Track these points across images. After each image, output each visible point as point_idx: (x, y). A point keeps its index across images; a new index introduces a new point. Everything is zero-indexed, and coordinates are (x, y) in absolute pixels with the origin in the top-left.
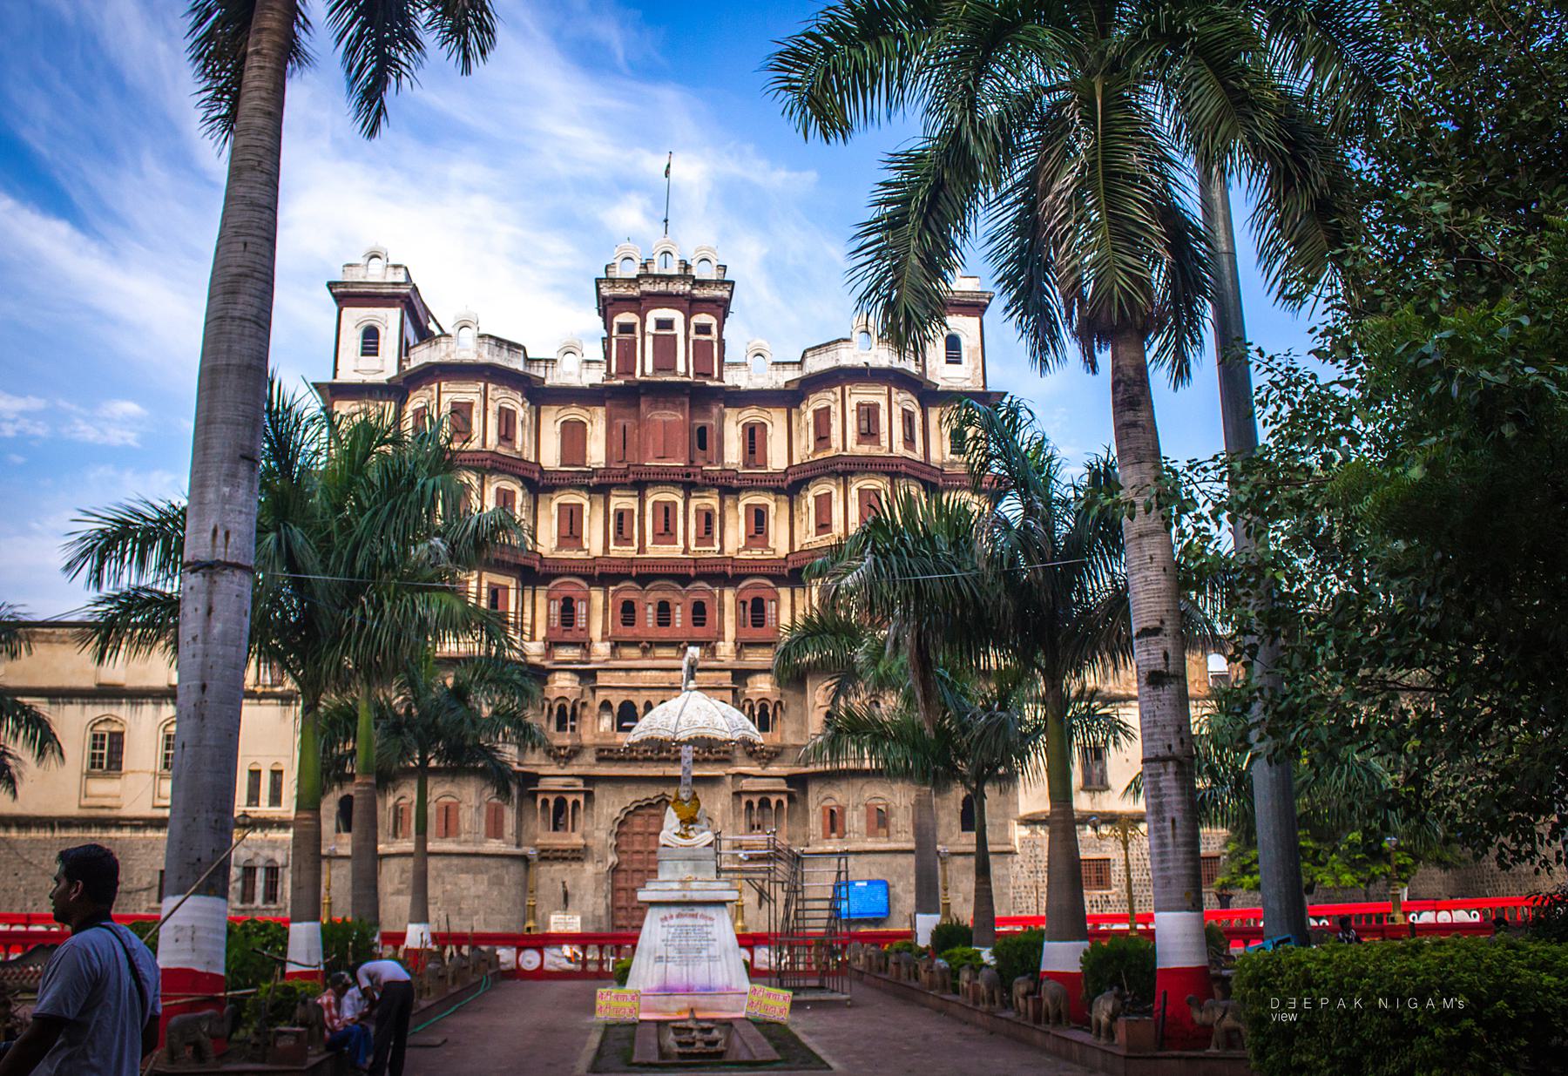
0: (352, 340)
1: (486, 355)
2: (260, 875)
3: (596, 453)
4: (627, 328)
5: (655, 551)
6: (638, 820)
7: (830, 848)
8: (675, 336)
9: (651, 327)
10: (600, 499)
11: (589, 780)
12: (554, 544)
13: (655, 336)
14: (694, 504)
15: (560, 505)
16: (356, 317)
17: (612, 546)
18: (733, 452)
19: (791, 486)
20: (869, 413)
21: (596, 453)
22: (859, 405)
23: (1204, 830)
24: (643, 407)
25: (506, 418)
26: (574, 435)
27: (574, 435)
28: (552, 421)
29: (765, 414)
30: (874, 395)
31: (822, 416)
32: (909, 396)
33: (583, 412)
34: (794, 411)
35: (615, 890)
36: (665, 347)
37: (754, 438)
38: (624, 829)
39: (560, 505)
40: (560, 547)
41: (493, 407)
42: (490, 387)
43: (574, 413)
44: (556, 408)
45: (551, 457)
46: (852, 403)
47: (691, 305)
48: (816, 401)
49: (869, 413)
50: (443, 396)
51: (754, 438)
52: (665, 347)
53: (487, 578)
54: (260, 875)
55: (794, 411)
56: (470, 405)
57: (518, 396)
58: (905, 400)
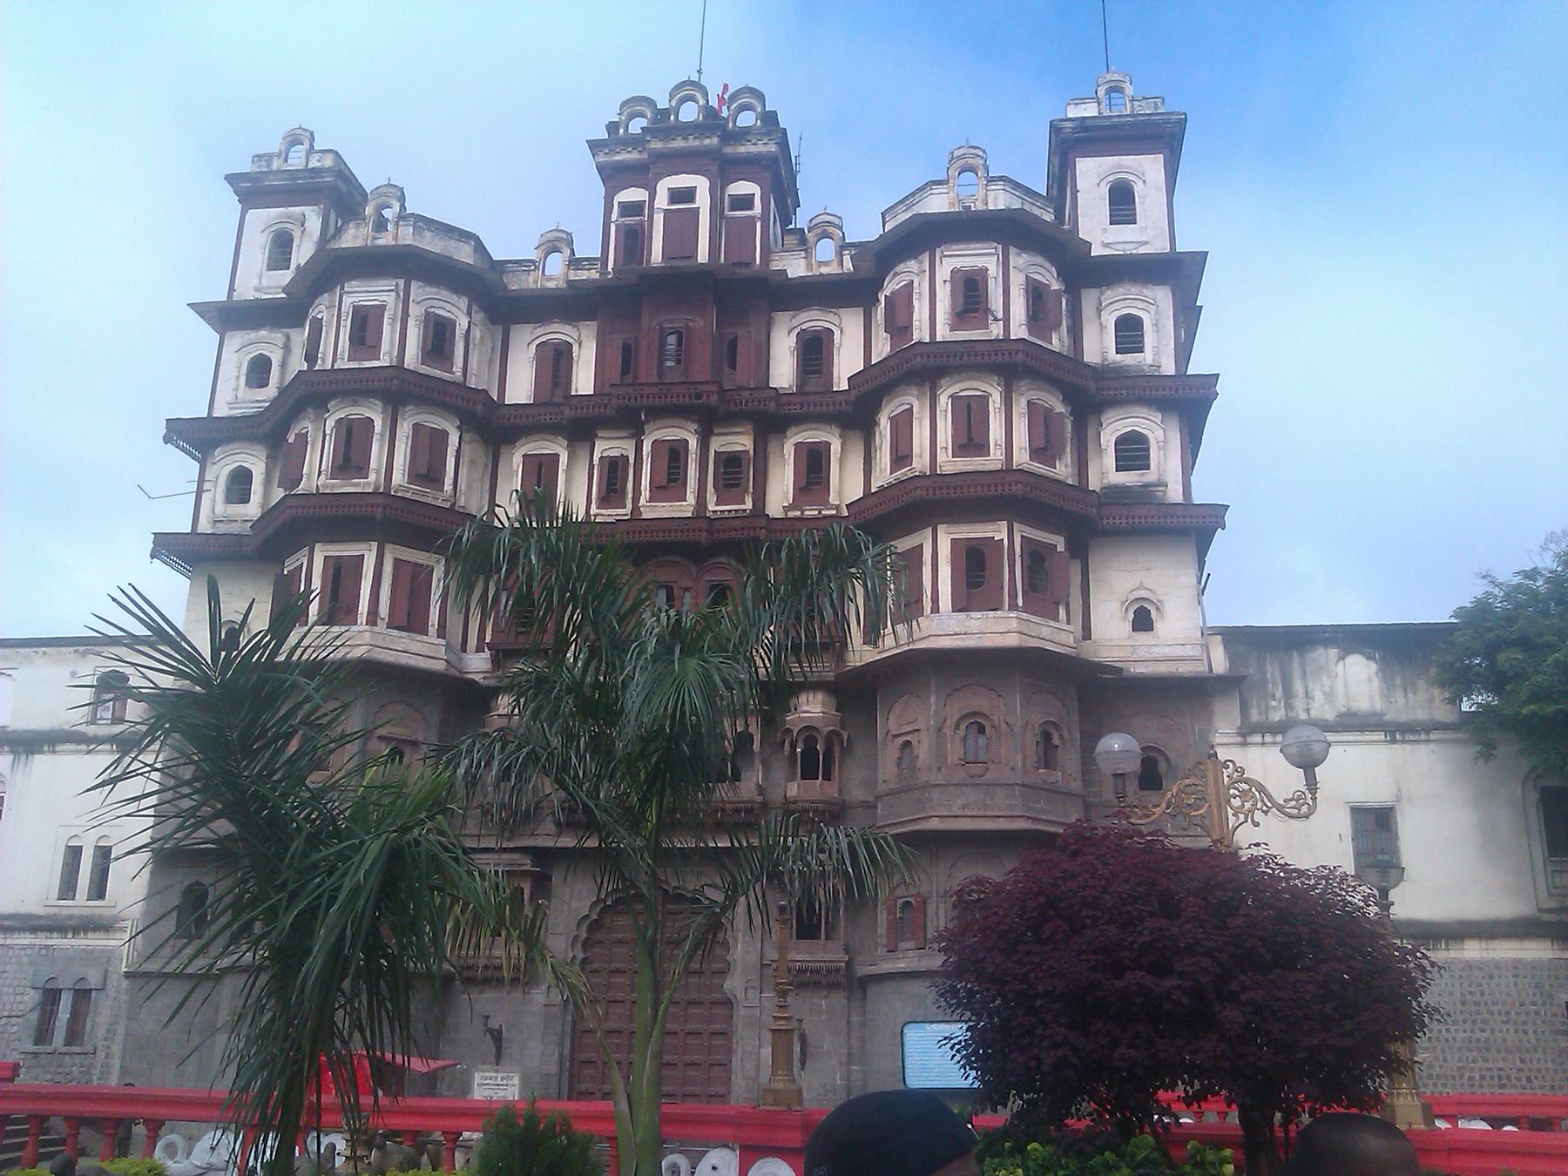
2: (66, 1001)
3: (584, 381)
5: (655, 510)
6: (622, 921)
7: (902, 966)
9: (662, 201)
11: (539, 854)
13: (666, 212)
14: (717, 444)
16: (262, 219)
17: (594, 510)
18: (783, 371)
19: (857, 413)
21: (584, 381)
23: (820, 696)
25: (439, 337)
26: (556, 362)
27: (556, 362)
29: (830, 317)
30: (982, 258)
33: (568, 329)
35: (579, 1034)
36: (681, 225)
37: (815, 351)
38: (599, 935)
41: (415, 311)
43: (559, 332)
45: (520, 388)
46: (944, 271)
47: (723, 169)
49: (971, 293)
51: (815, 351)
52: (681, 225)
54: (66, 1001)
58: (1026, 266)
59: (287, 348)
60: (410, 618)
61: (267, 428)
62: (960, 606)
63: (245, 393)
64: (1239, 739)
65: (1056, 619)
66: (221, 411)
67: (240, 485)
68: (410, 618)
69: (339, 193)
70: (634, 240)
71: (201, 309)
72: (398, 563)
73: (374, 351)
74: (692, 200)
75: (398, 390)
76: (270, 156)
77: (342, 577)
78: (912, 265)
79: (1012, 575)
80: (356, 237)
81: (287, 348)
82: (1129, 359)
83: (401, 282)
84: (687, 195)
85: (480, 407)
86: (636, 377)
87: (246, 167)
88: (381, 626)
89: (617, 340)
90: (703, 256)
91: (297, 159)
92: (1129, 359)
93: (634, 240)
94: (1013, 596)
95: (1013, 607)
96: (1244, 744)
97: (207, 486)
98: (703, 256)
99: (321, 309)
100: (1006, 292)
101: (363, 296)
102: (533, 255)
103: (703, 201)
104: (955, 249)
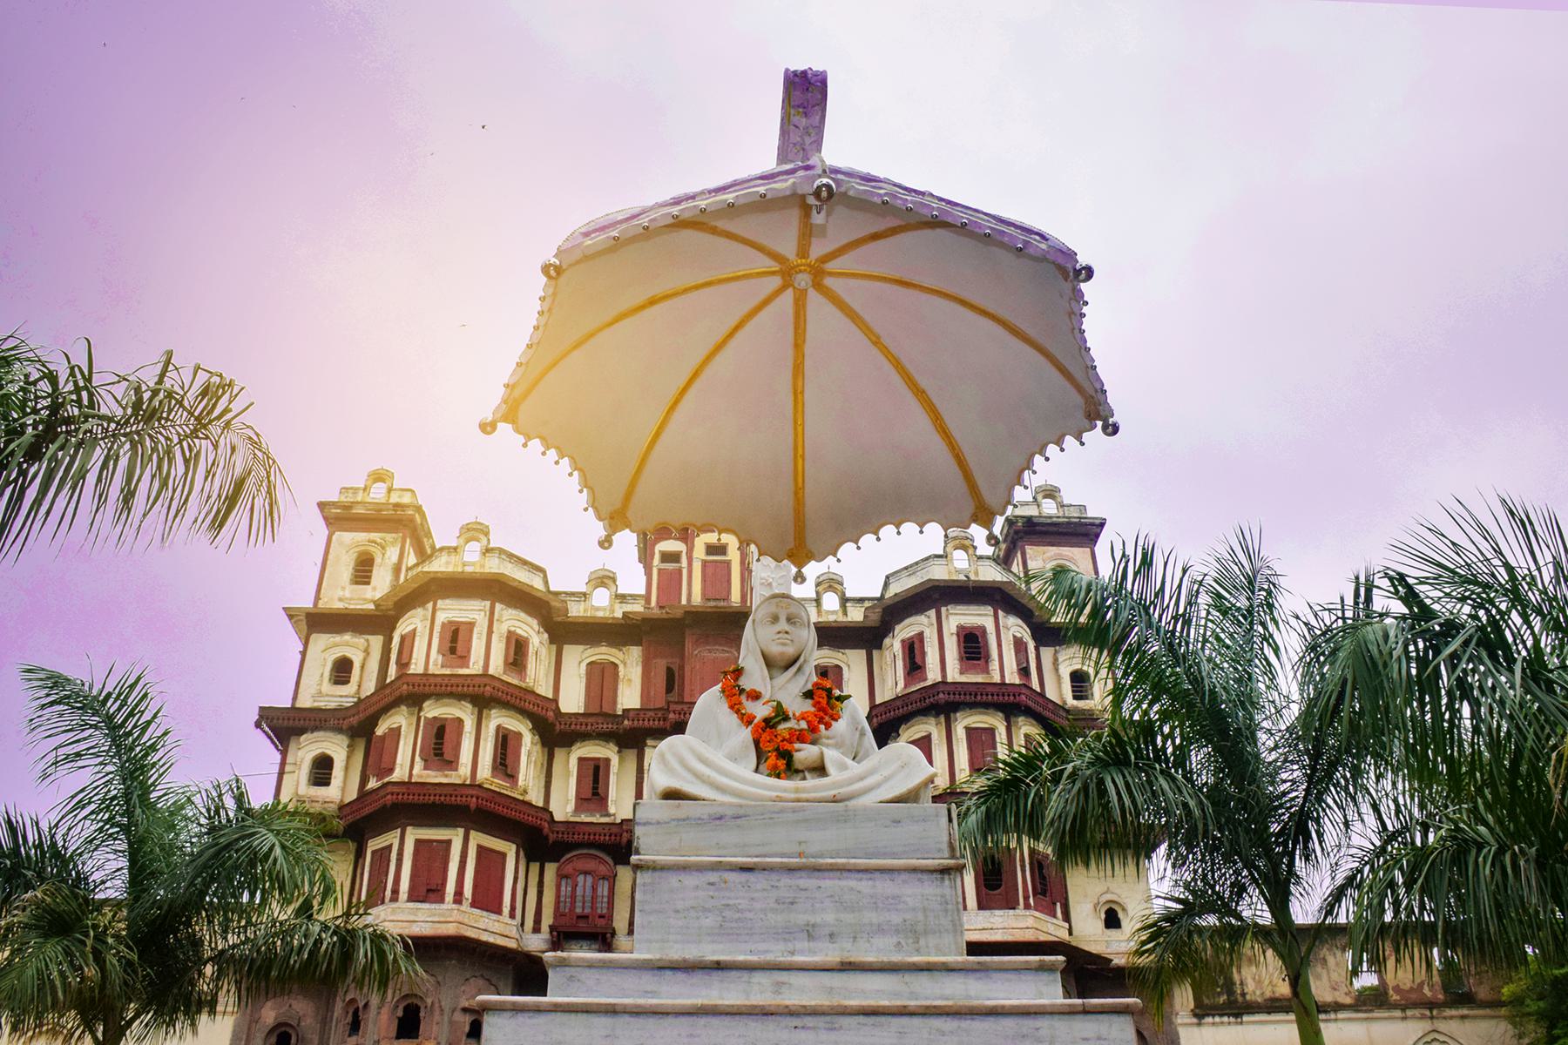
0: (343, 568)
1: (494, 566)
3: (629, 697)
4: (669, 557)
8: (728, 563)
10: (631, 755)
12: (571, 807)
15: (581, 760)
16: (350, 541)
20: (973, 645)
22: (961, 628)
24: (688, 645)
25: (518, 651)
26: (602, 679)
28: (577, 660)
30: (979, 616)
31: (913, 650)
32: (1020, 622)
33: (614, 651)
34: (875, 653)
39: (581, 760)
40: (578, 810)
41: (501, 629)
42: (498, 606)
43: (603, 653)
44: (581, 648)
45: (572, 700)
48: (905, 630)
50: (438, 614)
53: (477, 838)
55: (875, 653)
56: (471, 625)
57: (534, 623)
58: (1015, 627)
59: (367, 652)
60: (487, 898)
61: (354, 721)
62: (982, 906)
63: (327, 687)
64: (1195, 1020)
65: (1054, 916)
66: (305, 702)
67: (322, 770)
68: (487, 898)
69: (402, 521)
70: (671, 583)
71: (291, 614)
72: (481, 850)
73: (464, 659)
74: (724, 553)
75: (484, 696)
76: (355, 490)
77: (431, 860)
78: (922, 619)
79: (1023, 878)
80: (448, 563)
81: (367, 652)
82: (1081, 704)
83: (488, 603)
84: (717, 549)
85: (551, 714)
86: (681, 694)
87: (334, 497)
88: (466, 906)
89: (661, 665)
90: (697, 599)
91: (378, 493)
92: (1081, 704)
93: (671, 583)
94: (1026, 898)
95: (1027, 906)
96: (1199, 1024)
97: (287, 768)
98: (684, 602)
99: (413, 622)
100: (1000, 646)
101: (456, 613)
102: (583, 589)
103: (733, 555)
104: (961, 609)
